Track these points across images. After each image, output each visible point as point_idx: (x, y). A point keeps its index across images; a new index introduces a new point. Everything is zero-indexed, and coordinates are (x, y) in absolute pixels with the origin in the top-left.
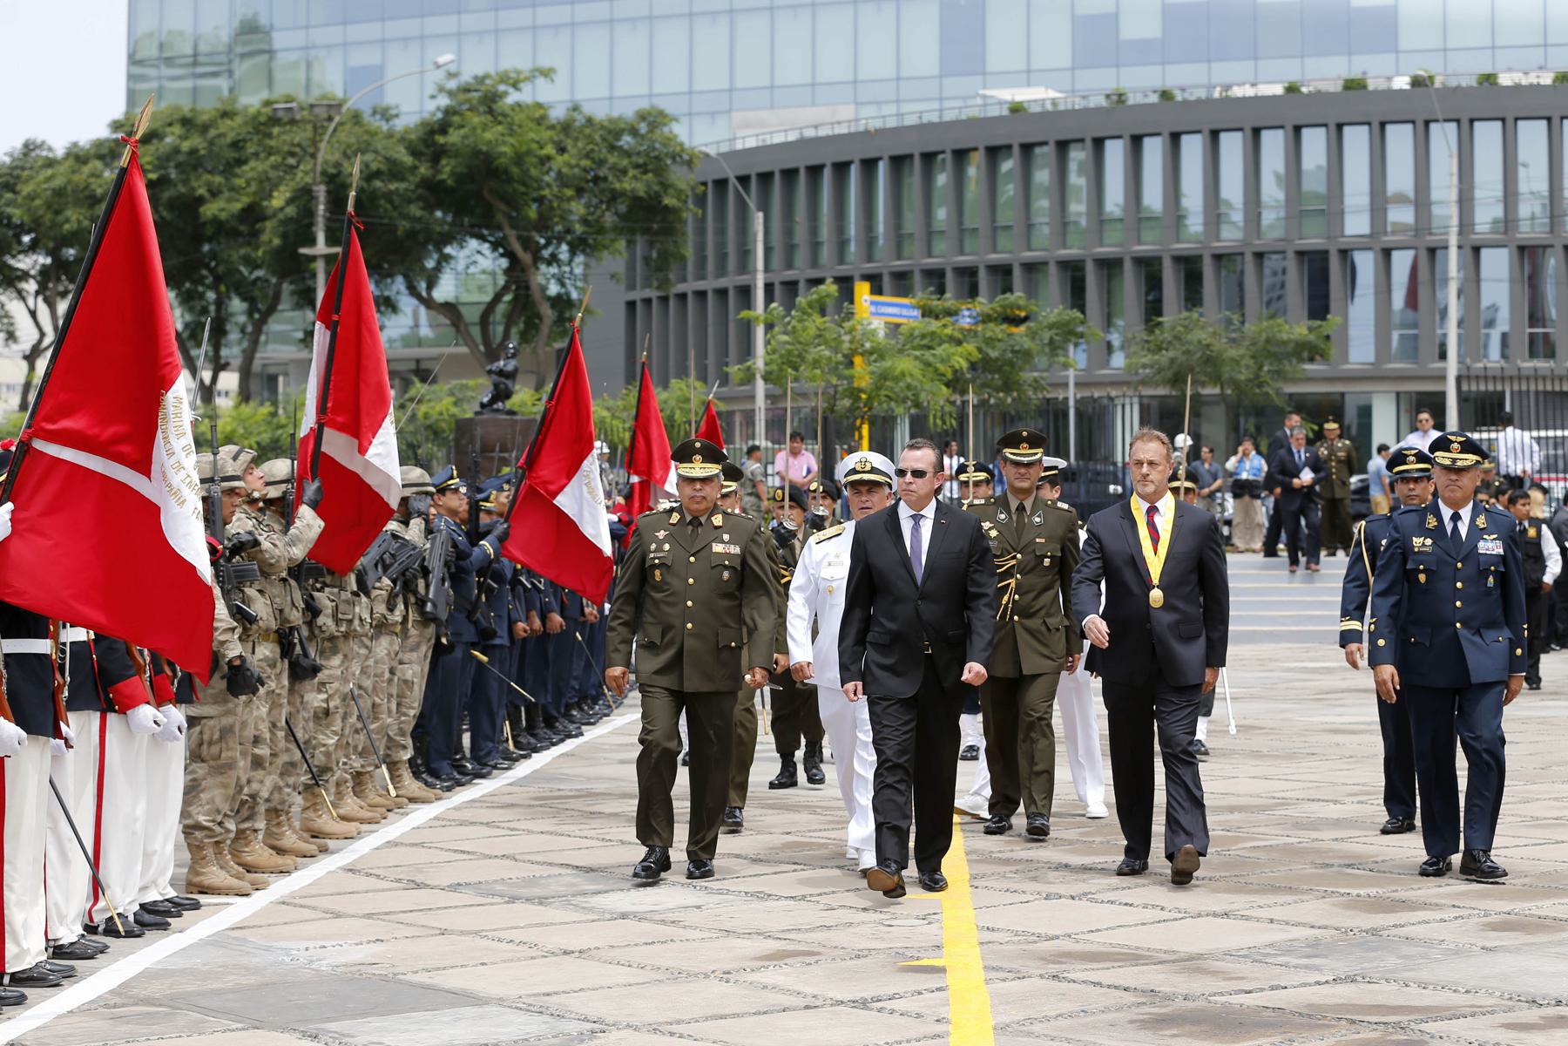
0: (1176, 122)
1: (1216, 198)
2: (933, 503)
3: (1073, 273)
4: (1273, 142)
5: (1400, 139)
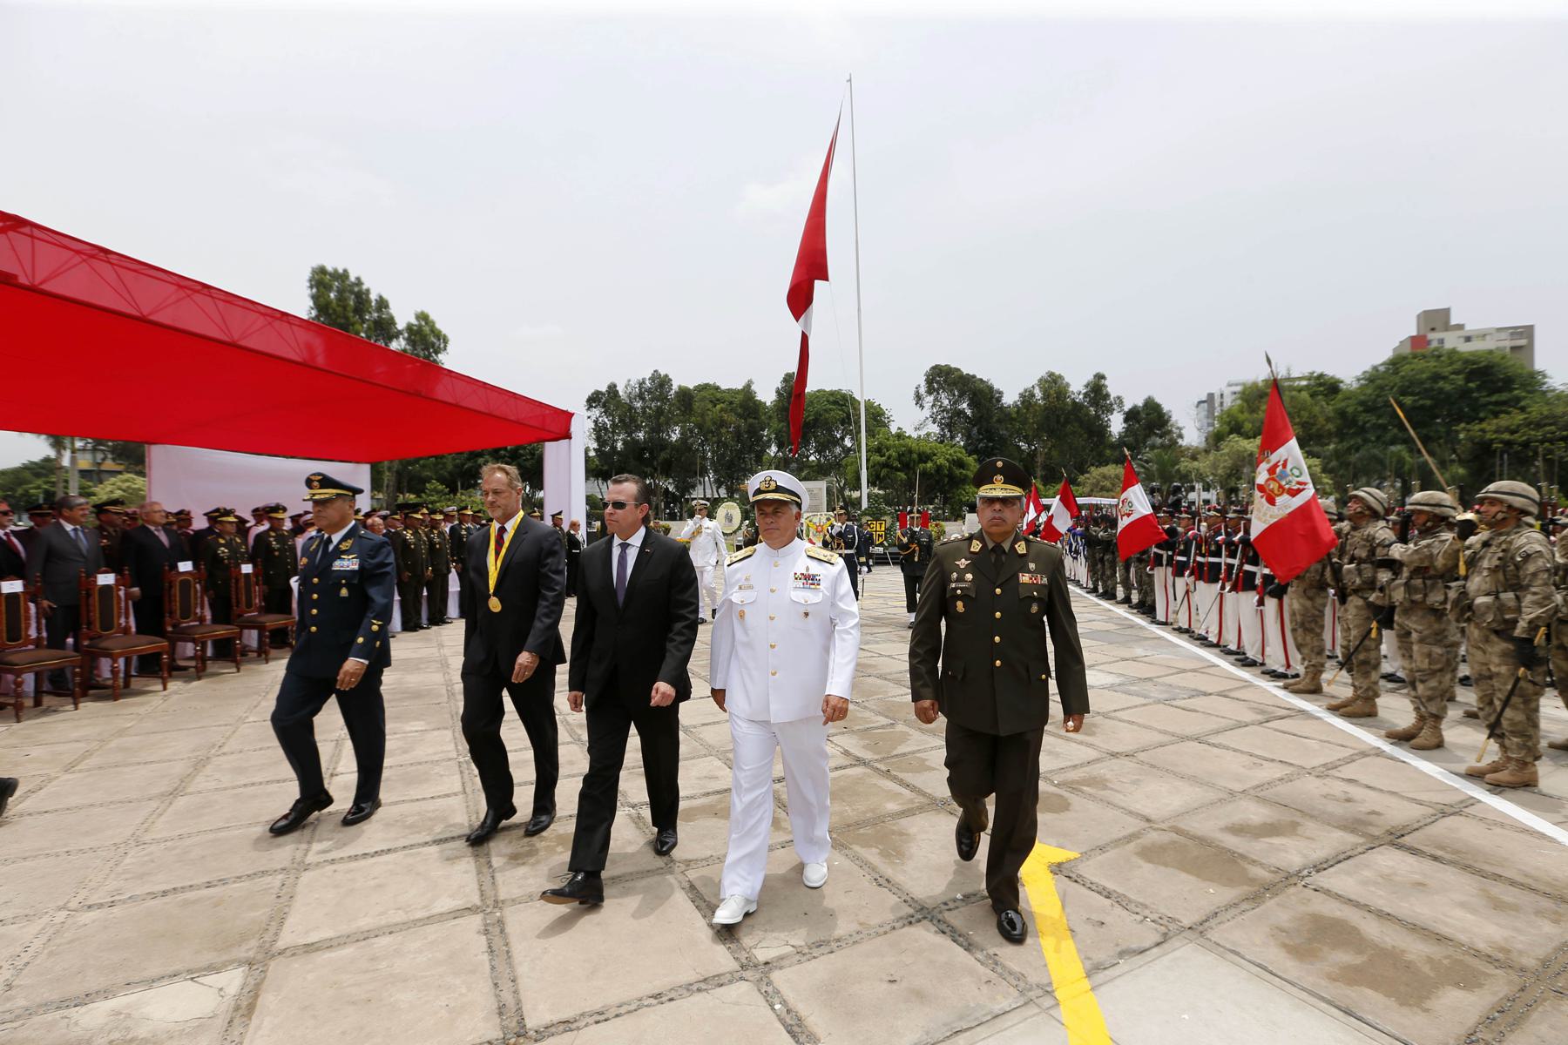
2: (642, 531)
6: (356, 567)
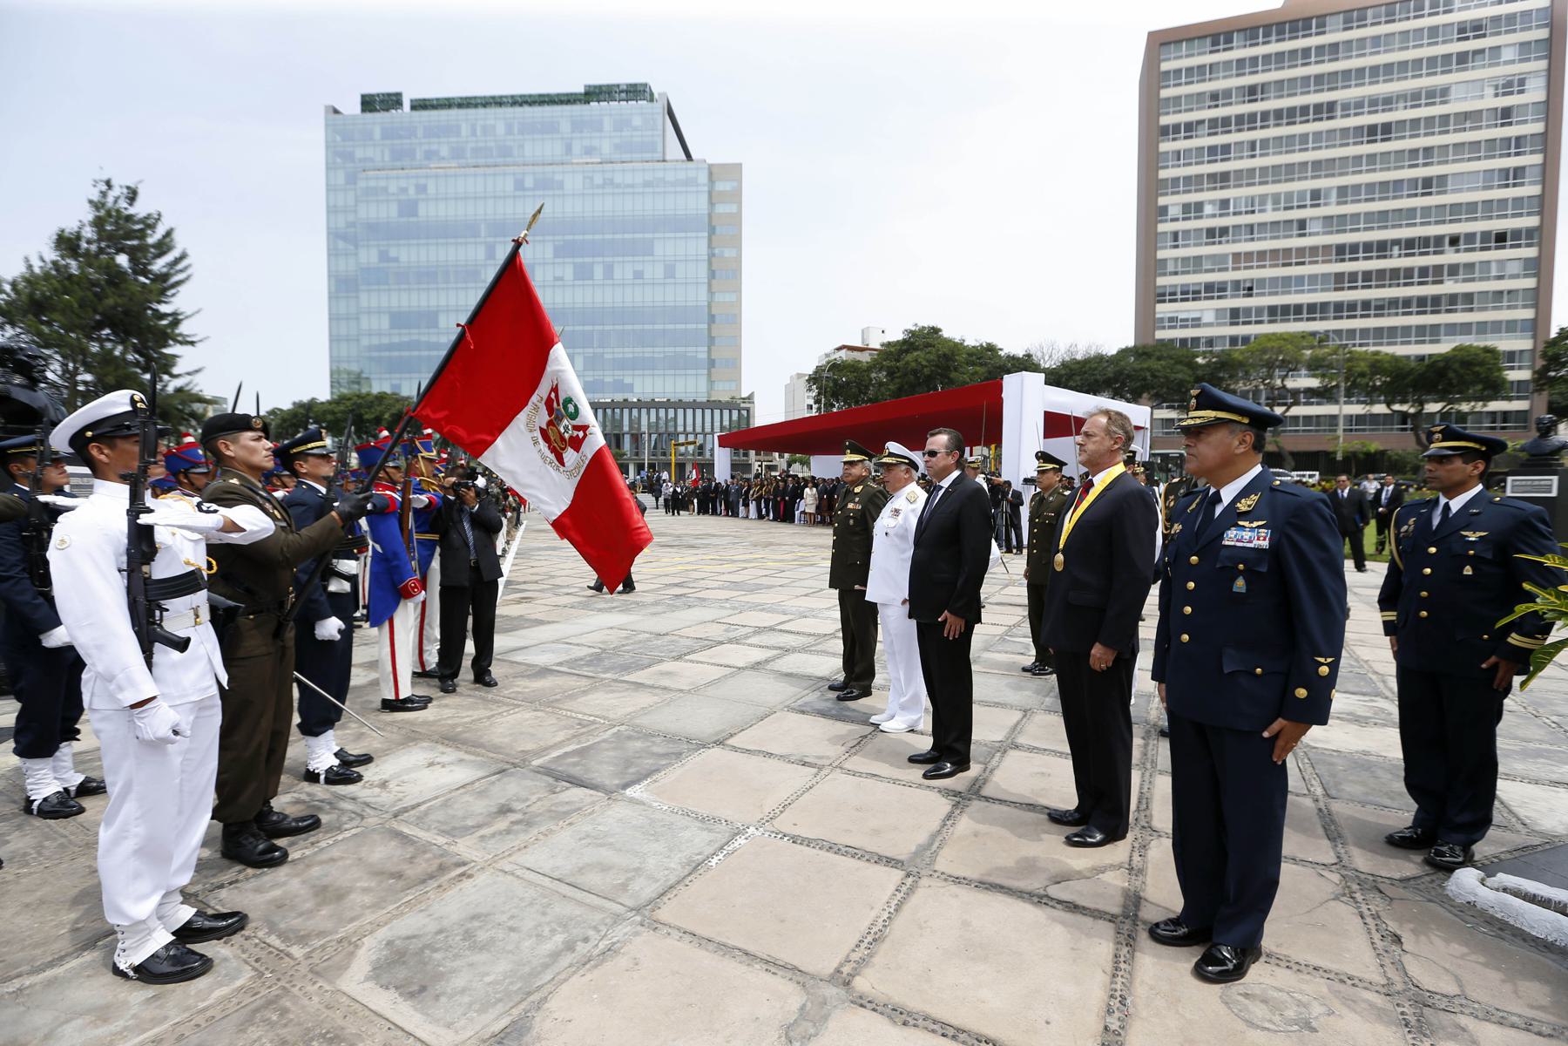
6: (1265, 544)
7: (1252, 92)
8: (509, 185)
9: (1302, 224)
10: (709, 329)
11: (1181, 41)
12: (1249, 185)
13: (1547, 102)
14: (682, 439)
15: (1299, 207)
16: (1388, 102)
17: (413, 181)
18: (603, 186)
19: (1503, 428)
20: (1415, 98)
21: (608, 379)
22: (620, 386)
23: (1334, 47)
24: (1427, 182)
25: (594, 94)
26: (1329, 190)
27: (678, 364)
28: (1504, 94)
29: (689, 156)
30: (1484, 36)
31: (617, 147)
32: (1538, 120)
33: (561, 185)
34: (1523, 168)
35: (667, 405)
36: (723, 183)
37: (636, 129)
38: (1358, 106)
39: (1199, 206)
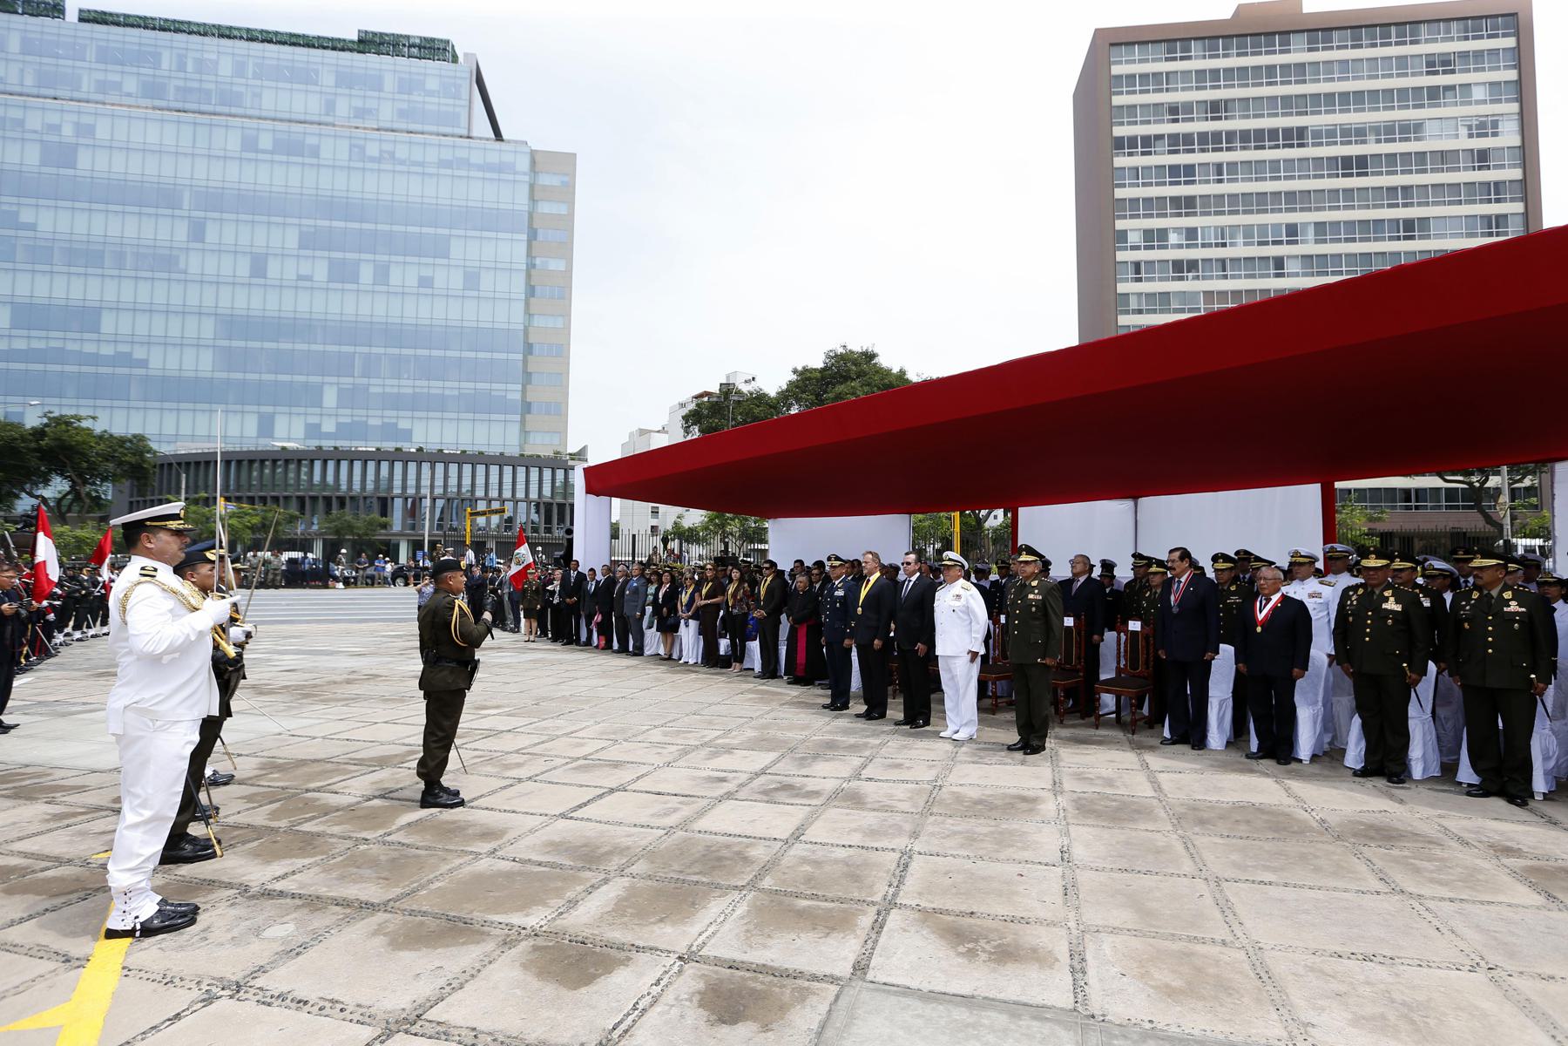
0: (338, 456)
1: (352, 480)
3: (301, 500)
4: (371, 465)
5: (412, 467)
7: (1216, 109)
8: (234, 142)
9: (1279, 262)
10: (525, 361)
11: (1133, 43)
12: (1217, 213)
13: (1523, 147)
14: (482, 506)
15: (1274, 243)
16: (1359, 134)
17: (74, 118)
18: (379, 160)
19: (1417, 508)
20: (1388, 132)
21: (373, 422)
22: (390, 430)
23: (1301, 67)
24: (1409, 224)
25: (369, 43)
26: (1305, 225)
27: (479, 406)
28: (1479, 135)
29: (498, 135)
30: (1453, 72)
31: (402, 114)
32: (1514, 166)
33: (315, 152)
34: (1506, 216)
35: (462, 459)
36: (550, 175)
37: (431, 93)
38: (1329, 136)
39: (1163, 234)
